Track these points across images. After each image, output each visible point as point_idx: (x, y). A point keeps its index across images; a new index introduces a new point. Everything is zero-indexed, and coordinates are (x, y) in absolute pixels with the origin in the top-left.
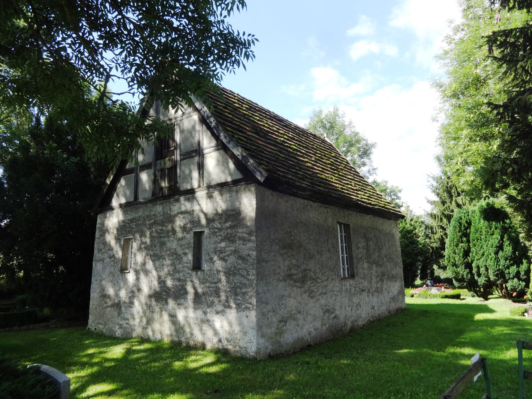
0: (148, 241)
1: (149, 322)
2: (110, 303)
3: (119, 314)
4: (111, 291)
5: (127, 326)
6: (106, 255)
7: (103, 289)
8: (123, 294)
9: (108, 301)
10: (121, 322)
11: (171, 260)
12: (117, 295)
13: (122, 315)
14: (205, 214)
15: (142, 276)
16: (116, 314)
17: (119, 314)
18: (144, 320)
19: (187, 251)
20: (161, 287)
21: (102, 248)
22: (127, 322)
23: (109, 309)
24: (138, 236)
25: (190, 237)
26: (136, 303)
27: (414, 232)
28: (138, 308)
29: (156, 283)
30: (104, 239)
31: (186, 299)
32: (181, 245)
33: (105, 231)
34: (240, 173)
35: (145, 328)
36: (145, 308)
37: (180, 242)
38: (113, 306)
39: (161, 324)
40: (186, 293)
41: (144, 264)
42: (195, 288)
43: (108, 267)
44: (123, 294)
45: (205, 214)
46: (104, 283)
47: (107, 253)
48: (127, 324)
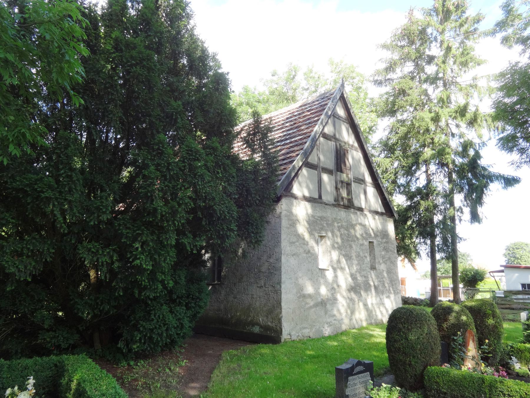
0: (339, 240)
1: (353, 312)
2: (312, 303)
3: (326, 313)
4: (310, 289)
5: (335, 322)
6: (301, 250)
7: (301, 289)
8: (323, 290)
9: (309, 300)
10: (329, 320)
11: (358, 261)
12: (318, 293)
13: (329, 313)
14: (372, 230)
15: (339, 273)
16: (323, 313)
17: (326, 313)
18: (349, 312)
19: (366, 255)
20: (354, 283)
21: (294, 241)
22: (334, 318)
23: (313, 310)
24: (330, 234)
25: (366, 243)
26: (339, 297)
27: (426, 143)
28: (342, 302)
29: (350, 279)
30: (296, 231)
31: (371, 290)
32: (363, 250)
33: (293, 222)
34: (377, 191)
35: (351, 320)
36: (348, 301)
37: (362, 247)
38: (316, 305)
39: (360, 313)
40: (370, 286)
41: (339, 261)
42: (374, 283)
43: (305, 264)
44: (323, 290)
45: (372, 230)
46: (300, 281)
47: (301, 247)
48: (335, 320)
